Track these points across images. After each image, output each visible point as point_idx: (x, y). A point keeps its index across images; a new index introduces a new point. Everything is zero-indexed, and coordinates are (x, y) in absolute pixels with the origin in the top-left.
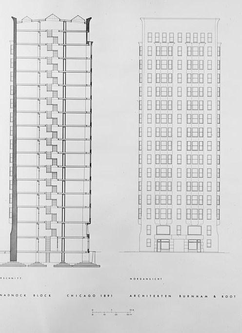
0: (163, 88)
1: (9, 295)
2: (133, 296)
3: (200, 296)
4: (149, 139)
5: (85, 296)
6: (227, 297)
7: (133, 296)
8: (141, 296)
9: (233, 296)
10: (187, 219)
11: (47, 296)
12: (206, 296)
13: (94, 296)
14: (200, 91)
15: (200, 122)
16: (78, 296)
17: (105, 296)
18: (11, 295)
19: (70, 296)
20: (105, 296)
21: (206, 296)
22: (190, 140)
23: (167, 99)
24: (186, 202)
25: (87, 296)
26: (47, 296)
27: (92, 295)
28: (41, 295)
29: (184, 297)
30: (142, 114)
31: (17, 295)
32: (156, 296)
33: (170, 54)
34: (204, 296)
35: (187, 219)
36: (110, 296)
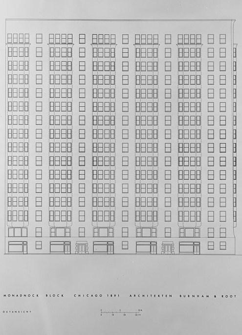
0: (185, 158)
1: (21, 296)
2: (133, 296)
3: (15, 295)
4: (211, 225)
5: (203, 296)
6: (227, 296)
7: (133, 296)
8: (141, 296)
9: (233, 296)
10: (179, 221)
11: (35, 295)
12: (5, 296)
13: (101, 296)
14: (139, 217)
15: (112, 165)
16: (85, 296)
17: (111, 296)
18: (23, 295)
19: (77, 296)
20: (111, 296)
21: (5, 296)
22: (139, 155)
23: (184, 167)
24: (178, 163)
25: (19, 296)
26: (35, 295)
27: (229, 296)
28: (54, 295)
29: (21, 296)
30: (234, 166)
31: (29, 296)
32: (157, 296)
33: (155, 123)
34: (205, 296)
35: (179, 221)
36: (109, 295)
